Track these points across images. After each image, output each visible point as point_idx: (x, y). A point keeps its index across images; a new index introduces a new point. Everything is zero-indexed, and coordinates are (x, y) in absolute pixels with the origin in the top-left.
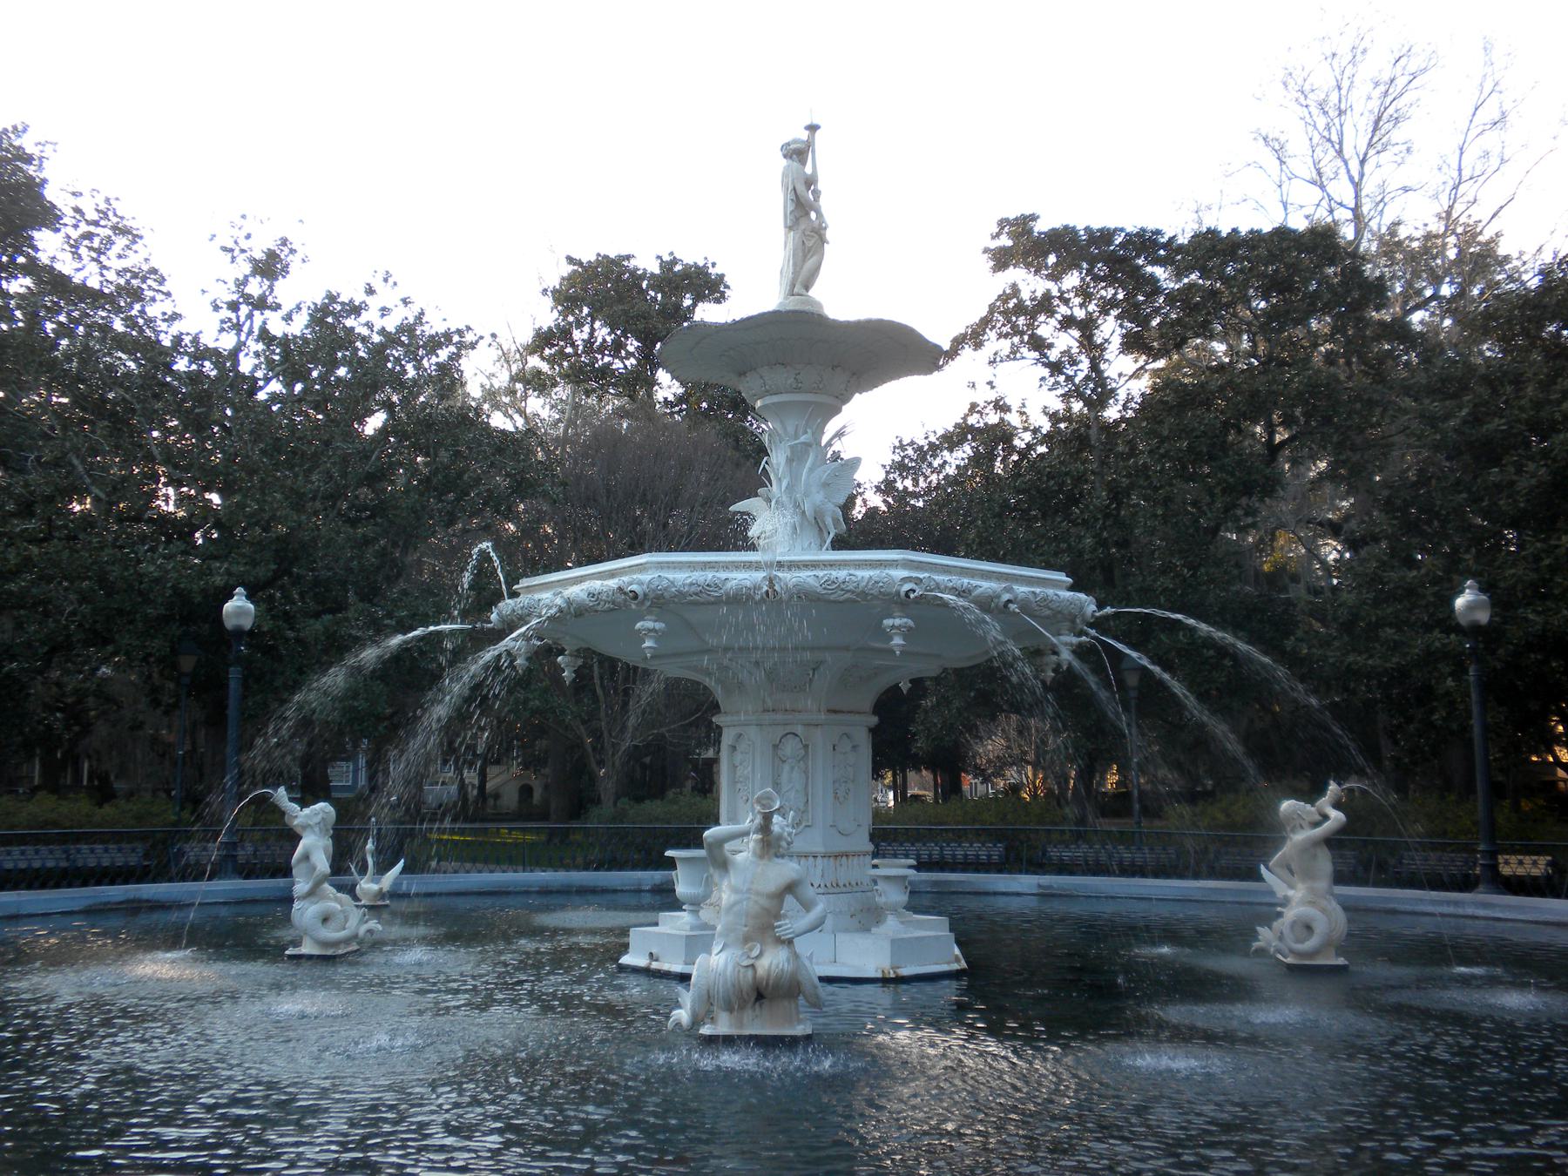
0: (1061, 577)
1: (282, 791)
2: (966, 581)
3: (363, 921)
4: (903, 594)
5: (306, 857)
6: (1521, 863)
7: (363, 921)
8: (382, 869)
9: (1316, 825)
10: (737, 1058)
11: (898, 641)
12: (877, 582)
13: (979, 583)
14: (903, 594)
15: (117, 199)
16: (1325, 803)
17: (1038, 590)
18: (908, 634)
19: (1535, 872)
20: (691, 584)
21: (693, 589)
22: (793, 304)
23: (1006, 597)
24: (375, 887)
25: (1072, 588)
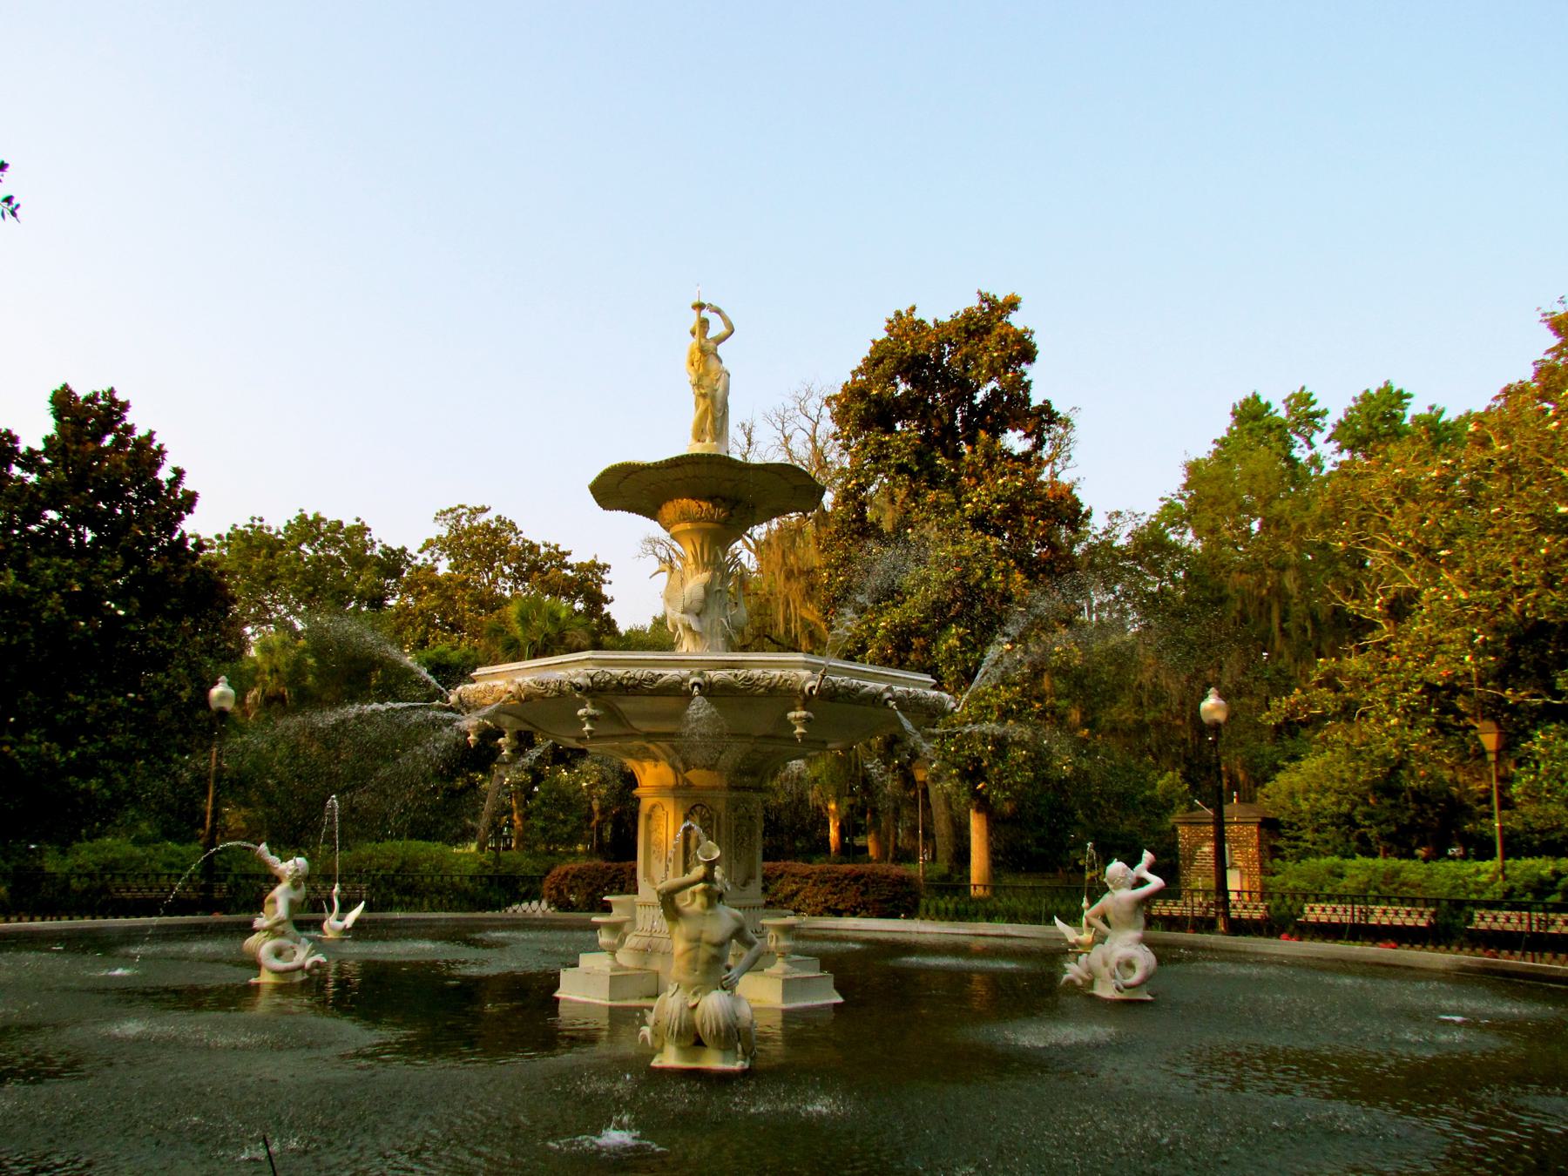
1: (264, 847)
2: (855, 681)
3: (309, 955)
4: (806, 690)
5: (274, 901)
6: (1384, 912)
7: (309, 955)
8: (346, 907)
9: (1134, 887)
10: (1485, 1004)
11: (799, 730)
12: (786, 680)
13: (662, 672)
14: (806, 690)
15: (743, 425)
16: (1141, 869)
17: (911, 690)
18: (807, 722)
19: (1422, 923)
20: (630, 678)
21: (631, 682)
22: (705, 447)
23: (887, 695)
24: (340, 925)
25: (934, 688)
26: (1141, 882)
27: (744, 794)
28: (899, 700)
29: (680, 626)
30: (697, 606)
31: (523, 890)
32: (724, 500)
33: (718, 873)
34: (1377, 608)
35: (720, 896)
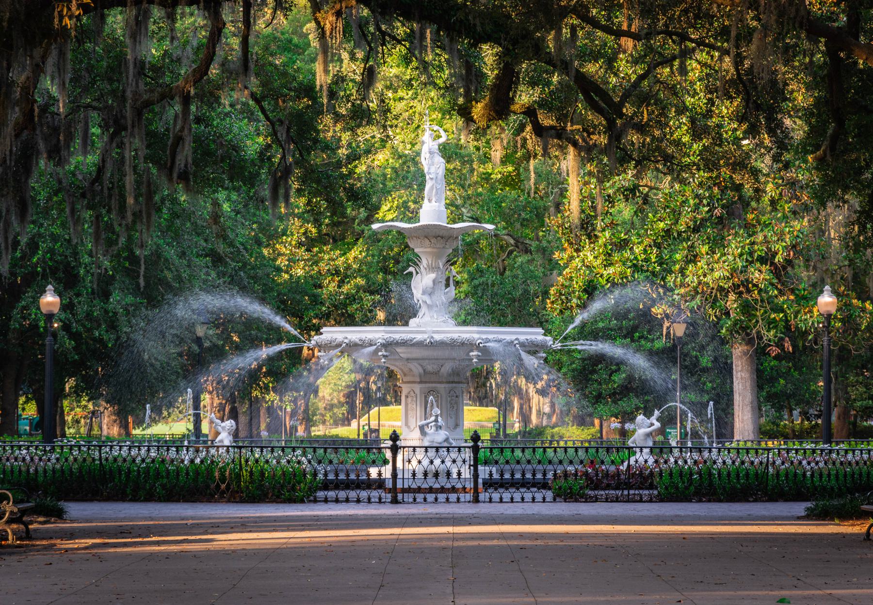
0: (540, 330)
11: (475, 360)
16: (653, 419)
23: (516, 342)
26: (652, 424)
27: (454, 385)
28: (522, 345)
29: (421, 302)
30: (430, 290)
31: (381, 186)
32: (442, 237)
33: (440, 419)
34: (545, 377)
35: (440, 427)
